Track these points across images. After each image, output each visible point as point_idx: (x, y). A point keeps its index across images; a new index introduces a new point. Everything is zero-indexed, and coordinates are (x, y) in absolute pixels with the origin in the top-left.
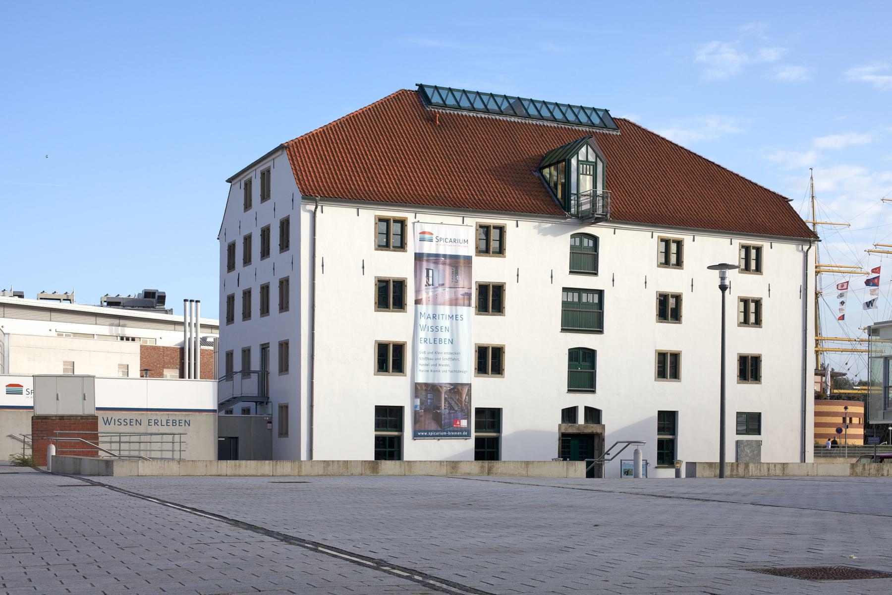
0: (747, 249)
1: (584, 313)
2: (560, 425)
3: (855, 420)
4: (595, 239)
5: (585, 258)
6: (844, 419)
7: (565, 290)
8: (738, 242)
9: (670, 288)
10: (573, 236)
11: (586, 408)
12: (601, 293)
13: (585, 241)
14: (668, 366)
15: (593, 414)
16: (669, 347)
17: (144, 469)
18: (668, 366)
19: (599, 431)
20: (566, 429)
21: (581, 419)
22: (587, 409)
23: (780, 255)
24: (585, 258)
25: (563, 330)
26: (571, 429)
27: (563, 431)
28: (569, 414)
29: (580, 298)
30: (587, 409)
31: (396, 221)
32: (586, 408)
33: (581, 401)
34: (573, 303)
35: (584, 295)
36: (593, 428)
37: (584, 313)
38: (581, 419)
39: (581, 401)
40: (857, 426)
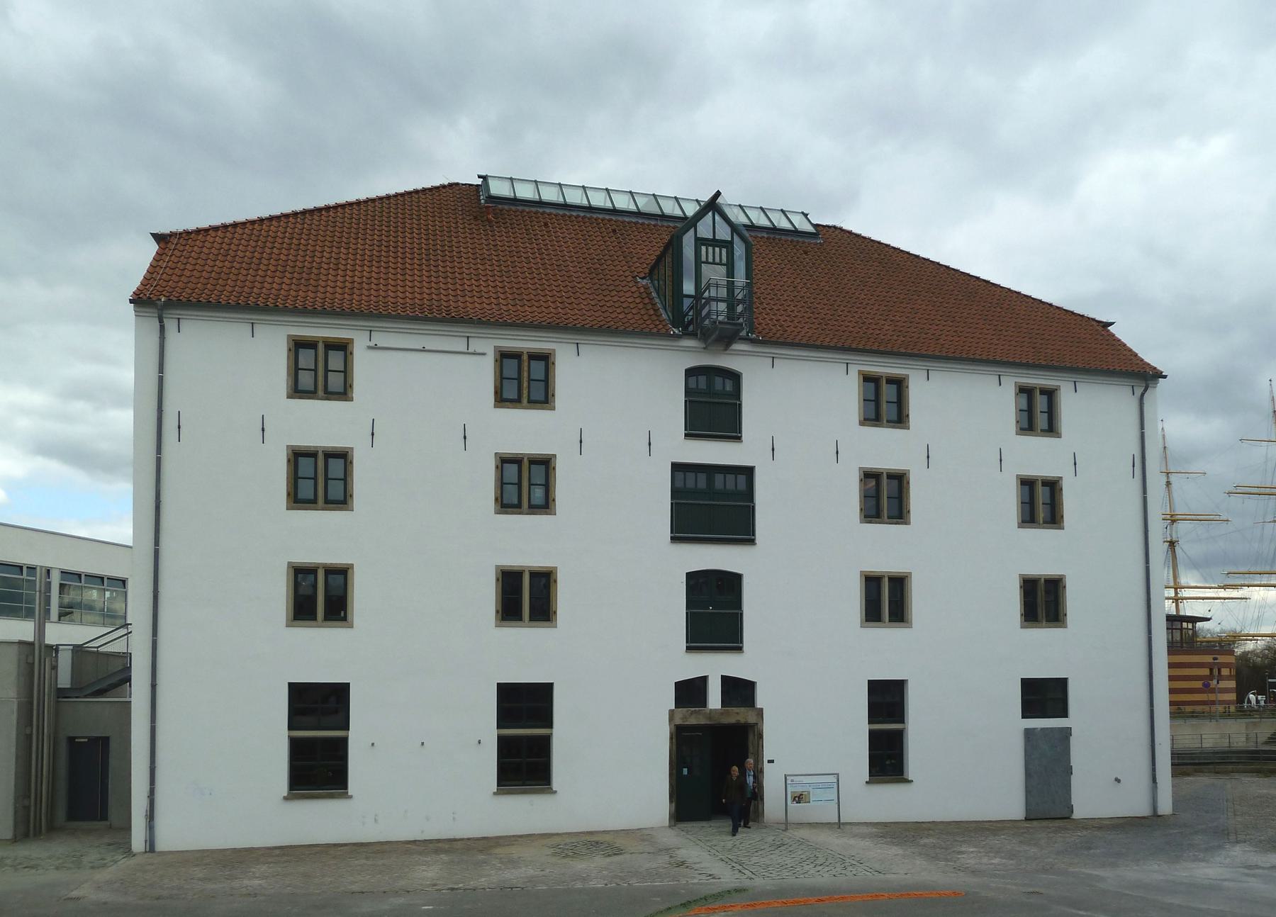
0: (1024, 391)
1: (713, 505)
2: (671, 713)
3: (1225, 672)
4: (735, 377)
5: (713, 407)
6: (1211, 670)
7: (676, 467)
8: (488, 345)
9: (886, 462)
10: (690, 373)
11: (725, 680)
12: (749, 472)
13: (718, 381)
14: (1043, 601)
15: (740, 691)
16: (1043, 568)
17: (888, 876)
18: (1043, 601)
19: (751, 719)
20: (684, 718)
21: (714, 699)
22: (727, 681)
23: (1088, 408)
24: (713, 407)
25: (674, 539)
26: (693, 718)
27: (678, 721)
28: (690, 692)
29: (710, 481)
30: (727, 681)
31: (534, 356)
32: (725, 680)
33: (715, 667)
34: (695, 493)
35: (719, 478)
36: (740, 715)
37: (713, 505)
38: (714, 699)
39: (715, 667)
40: (1229, 678)
